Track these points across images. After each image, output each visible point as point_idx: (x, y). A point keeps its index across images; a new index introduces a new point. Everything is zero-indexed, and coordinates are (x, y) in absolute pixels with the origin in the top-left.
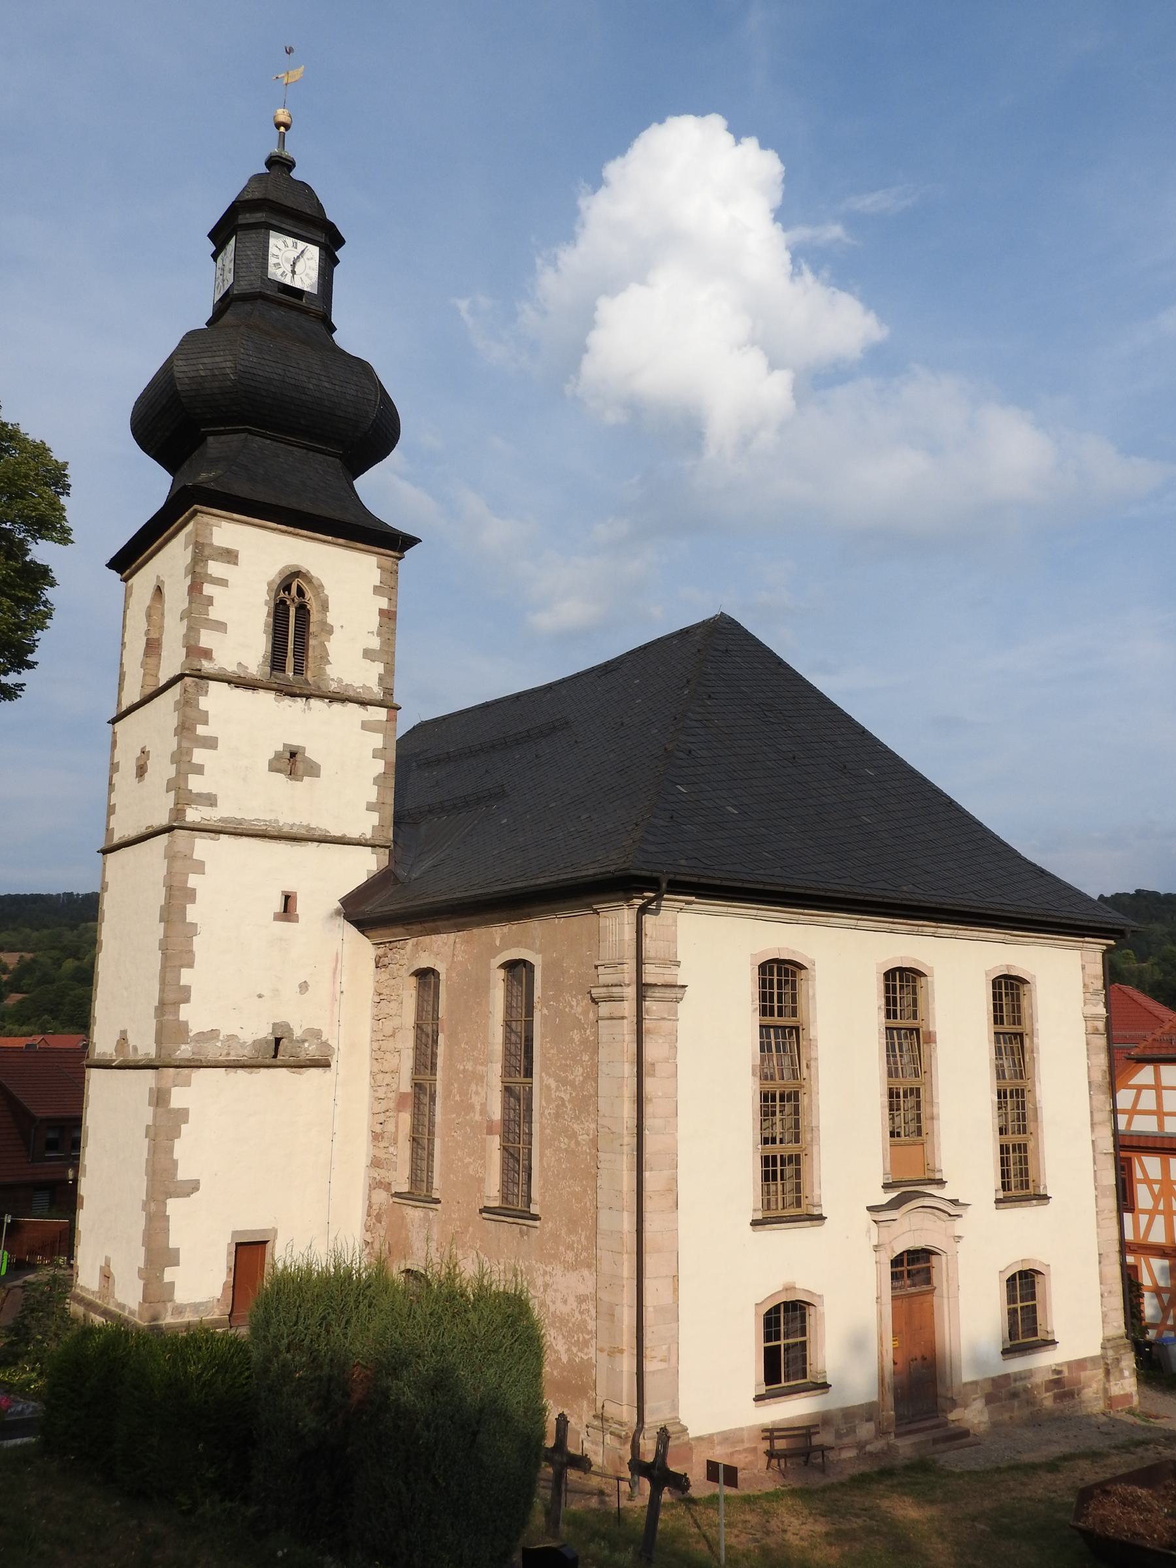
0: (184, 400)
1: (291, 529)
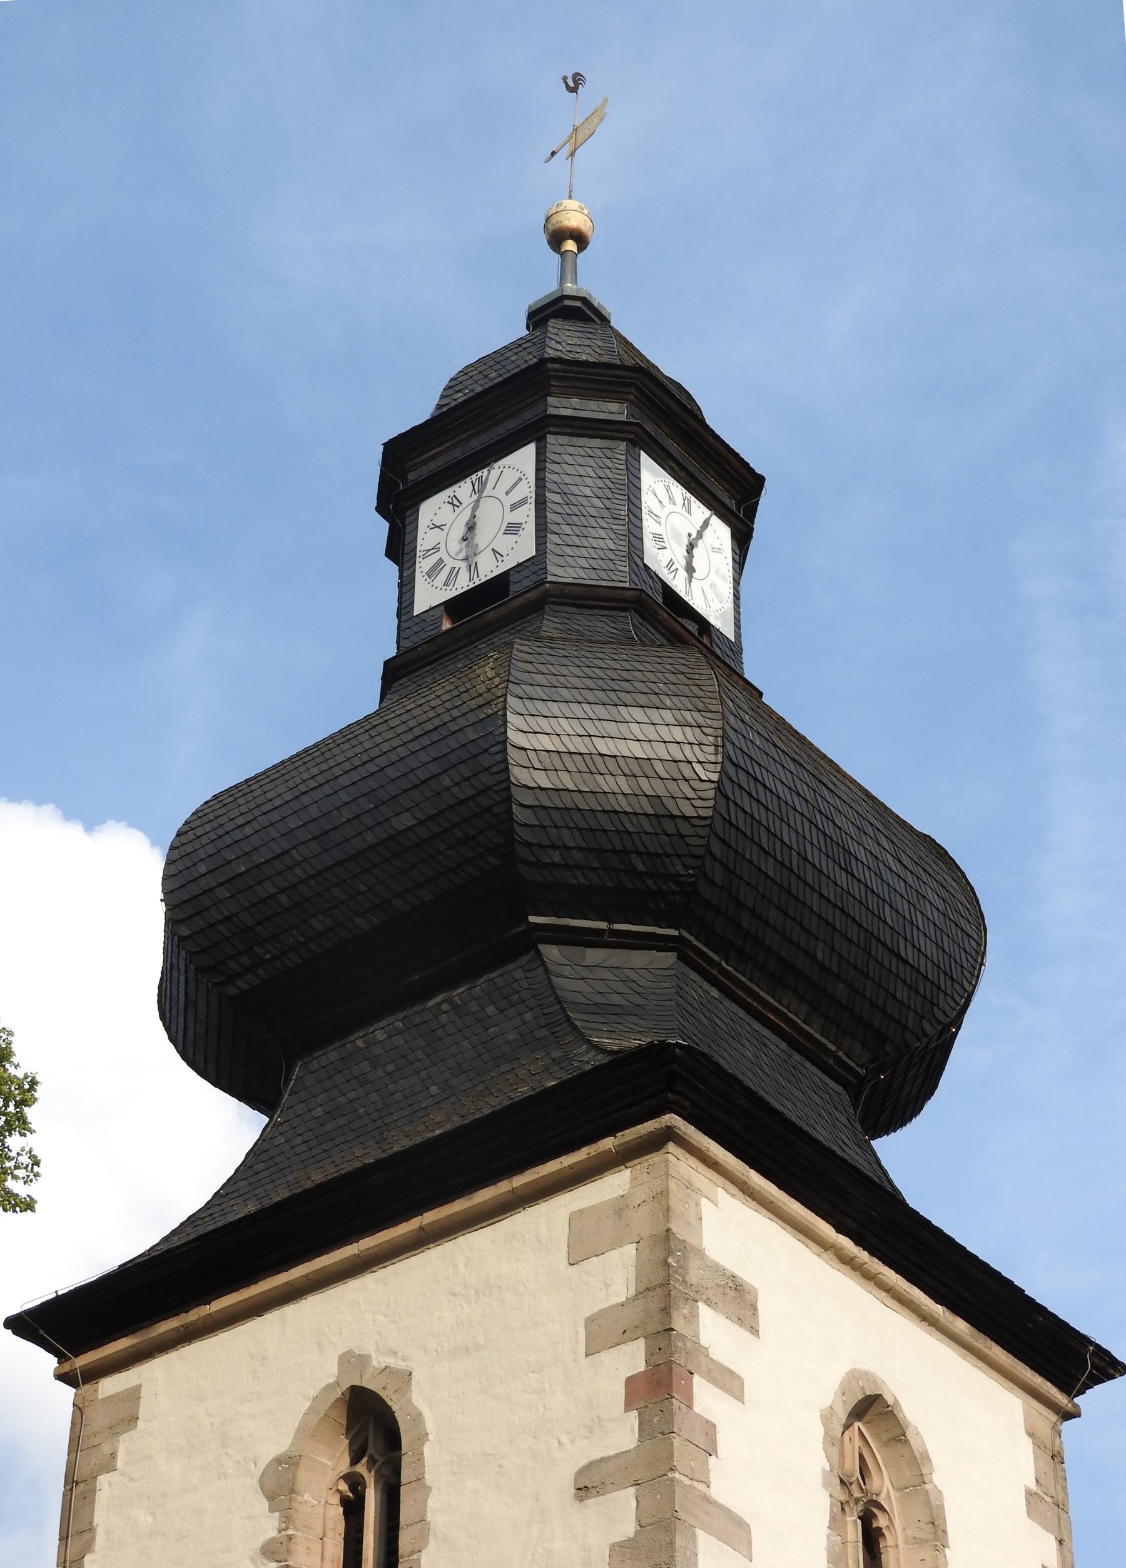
0: (518, 813)
1: (863, 1256)
